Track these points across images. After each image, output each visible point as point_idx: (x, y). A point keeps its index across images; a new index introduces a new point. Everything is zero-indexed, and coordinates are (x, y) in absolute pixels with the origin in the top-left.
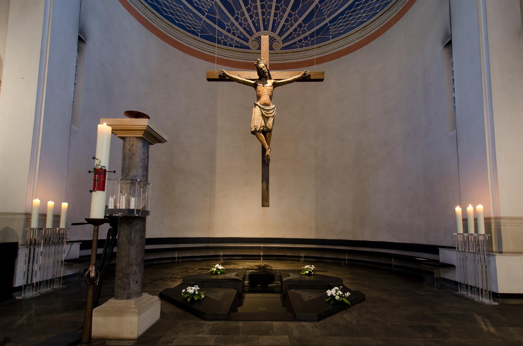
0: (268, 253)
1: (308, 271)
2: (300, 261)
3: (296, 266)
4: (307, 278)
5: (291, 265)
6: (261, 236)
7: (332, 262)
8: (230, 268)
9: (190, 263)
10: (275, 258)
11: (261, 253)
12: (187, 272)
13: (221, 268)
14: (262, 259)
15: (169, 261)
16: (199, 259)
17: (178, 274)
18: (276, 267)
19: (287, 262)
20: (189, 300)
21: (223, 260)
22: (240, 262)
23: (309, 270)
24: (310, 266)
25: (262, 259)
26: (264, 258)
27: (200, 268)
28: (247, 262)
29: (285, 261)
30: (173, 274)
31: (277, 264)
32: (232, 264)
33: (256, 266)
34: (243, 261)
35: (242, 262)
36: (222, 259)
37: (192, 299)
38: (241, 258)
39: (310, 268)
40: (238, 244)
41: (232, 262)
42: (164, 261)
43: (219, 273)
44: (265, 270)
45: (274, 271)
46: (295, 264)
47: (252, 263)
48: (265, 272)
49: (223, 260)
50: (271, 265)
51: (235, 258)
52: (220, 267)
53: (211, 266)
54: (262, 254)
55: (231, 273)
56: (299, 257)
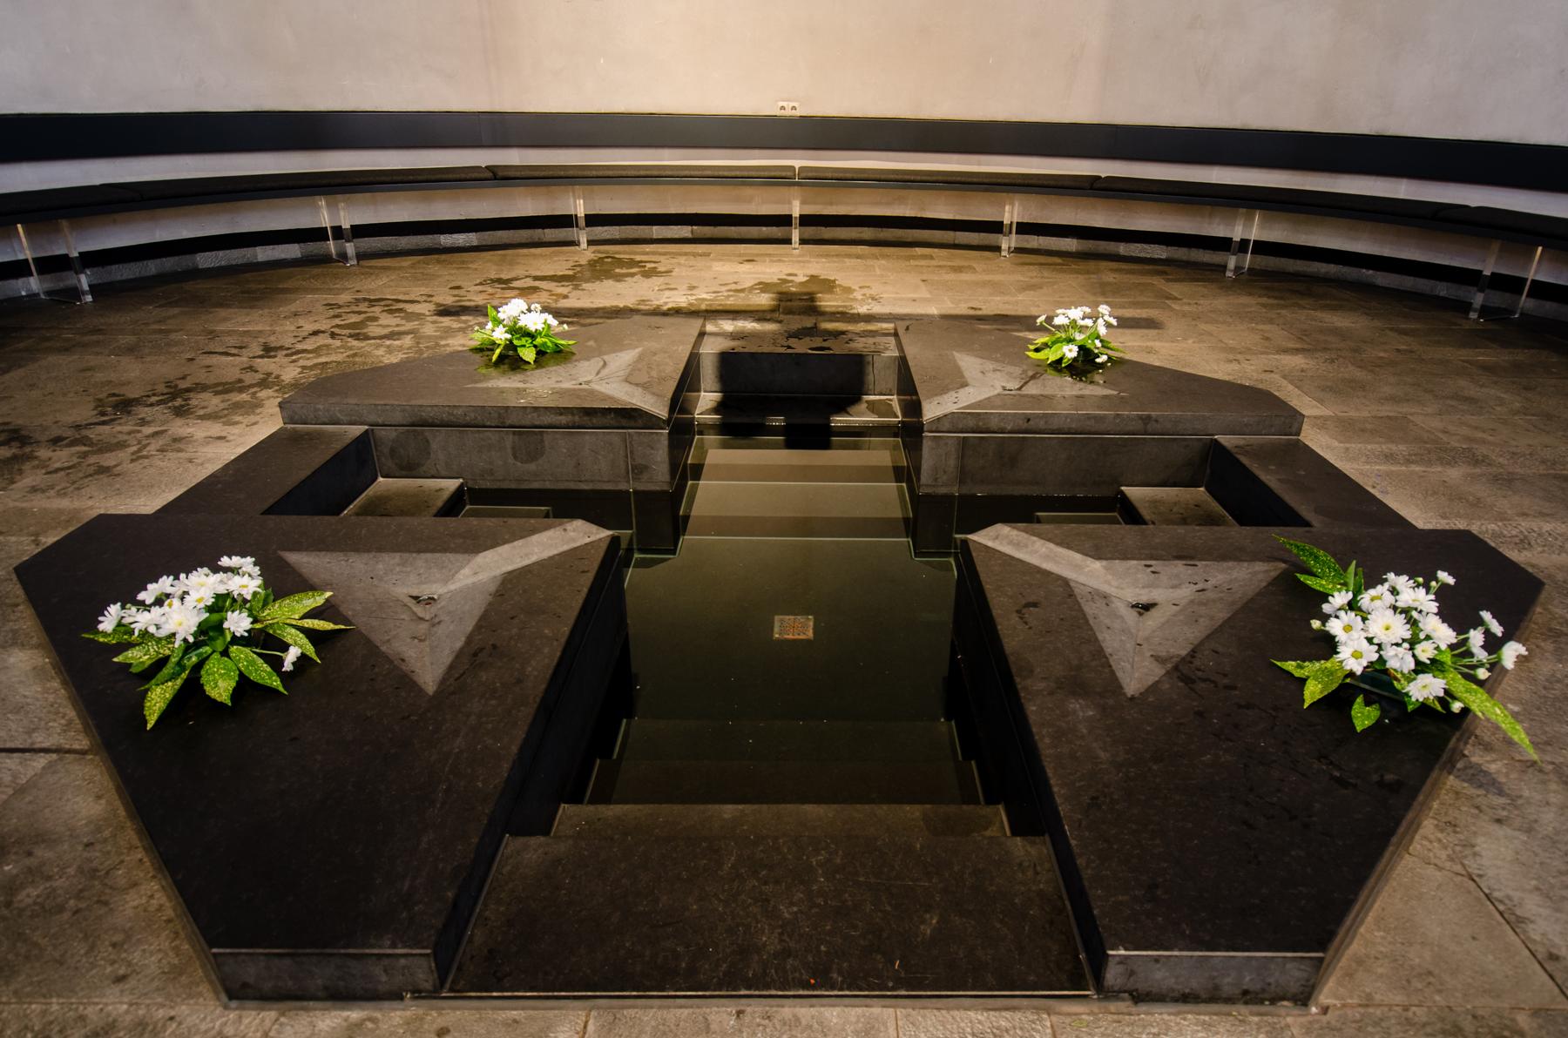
0: (831, 204)
1: (1070, 341)
2: (998, 249)
3: (984, 284)
4: (1066, 387)
5: (952, 276)
6: (794, 108)
7: (1164, 256)
8: (615, 303)
9: (407, 262)
10: (867, 233)
11: (790, 203)
12: (356, 337)
13: (540, 327)
14: (796, 235)
15: (292, 251)
16: (461, 239)
17: (299, 347)
18: (873, 292)
19: (931, 258)
20: (158, 698)
21: (590, 243)
22: (682, 260)
23: (1079, 337)
24: (1088, 310)
25: (796, 235)
26: (811, 231)
27: (448, 300)
28: (721, 258)
29: (919, 251)
30: (269, 351)
31: (878, 272)
32: (632, 275)
33: (764, 287)
34: (695, 255)
35: (692, 261)
36: (583, 240)
37: (186, 681)
38: (689, 235)
39: (1089, 322)
40: (666, 152)
41: (638, 258)
42: (263, 254)
43: (528, 354)
44: (808, 322)
45: (862, 327)
46: (971, 269)
47: (747, 267)
48: (812, 332)
49: (590, 243)
50: (846, 283)
51: (657, 231)
52: (535, 321)
53: (516, 284)
54: (796, 213)
55: (606, 357)
56: (996, 227)
